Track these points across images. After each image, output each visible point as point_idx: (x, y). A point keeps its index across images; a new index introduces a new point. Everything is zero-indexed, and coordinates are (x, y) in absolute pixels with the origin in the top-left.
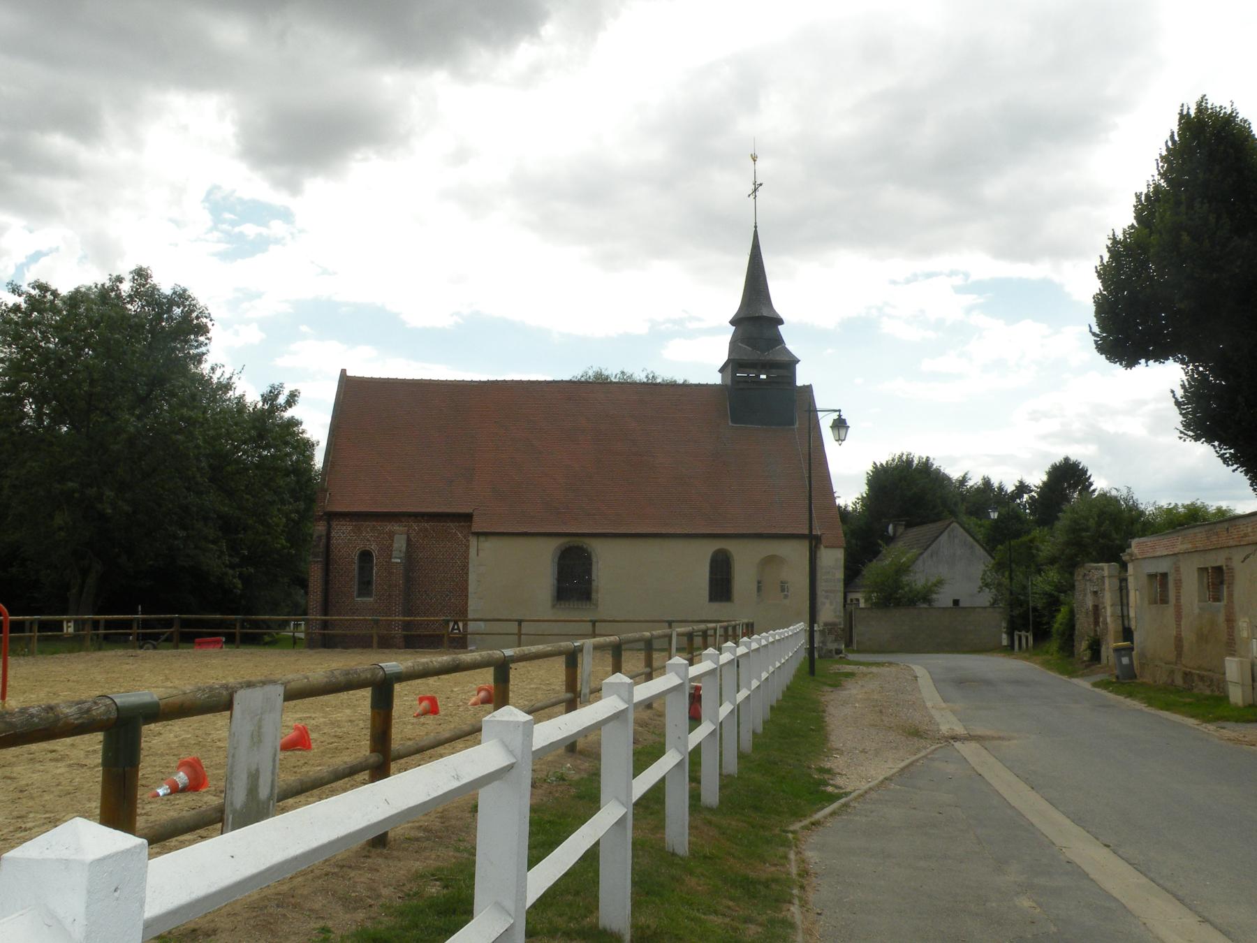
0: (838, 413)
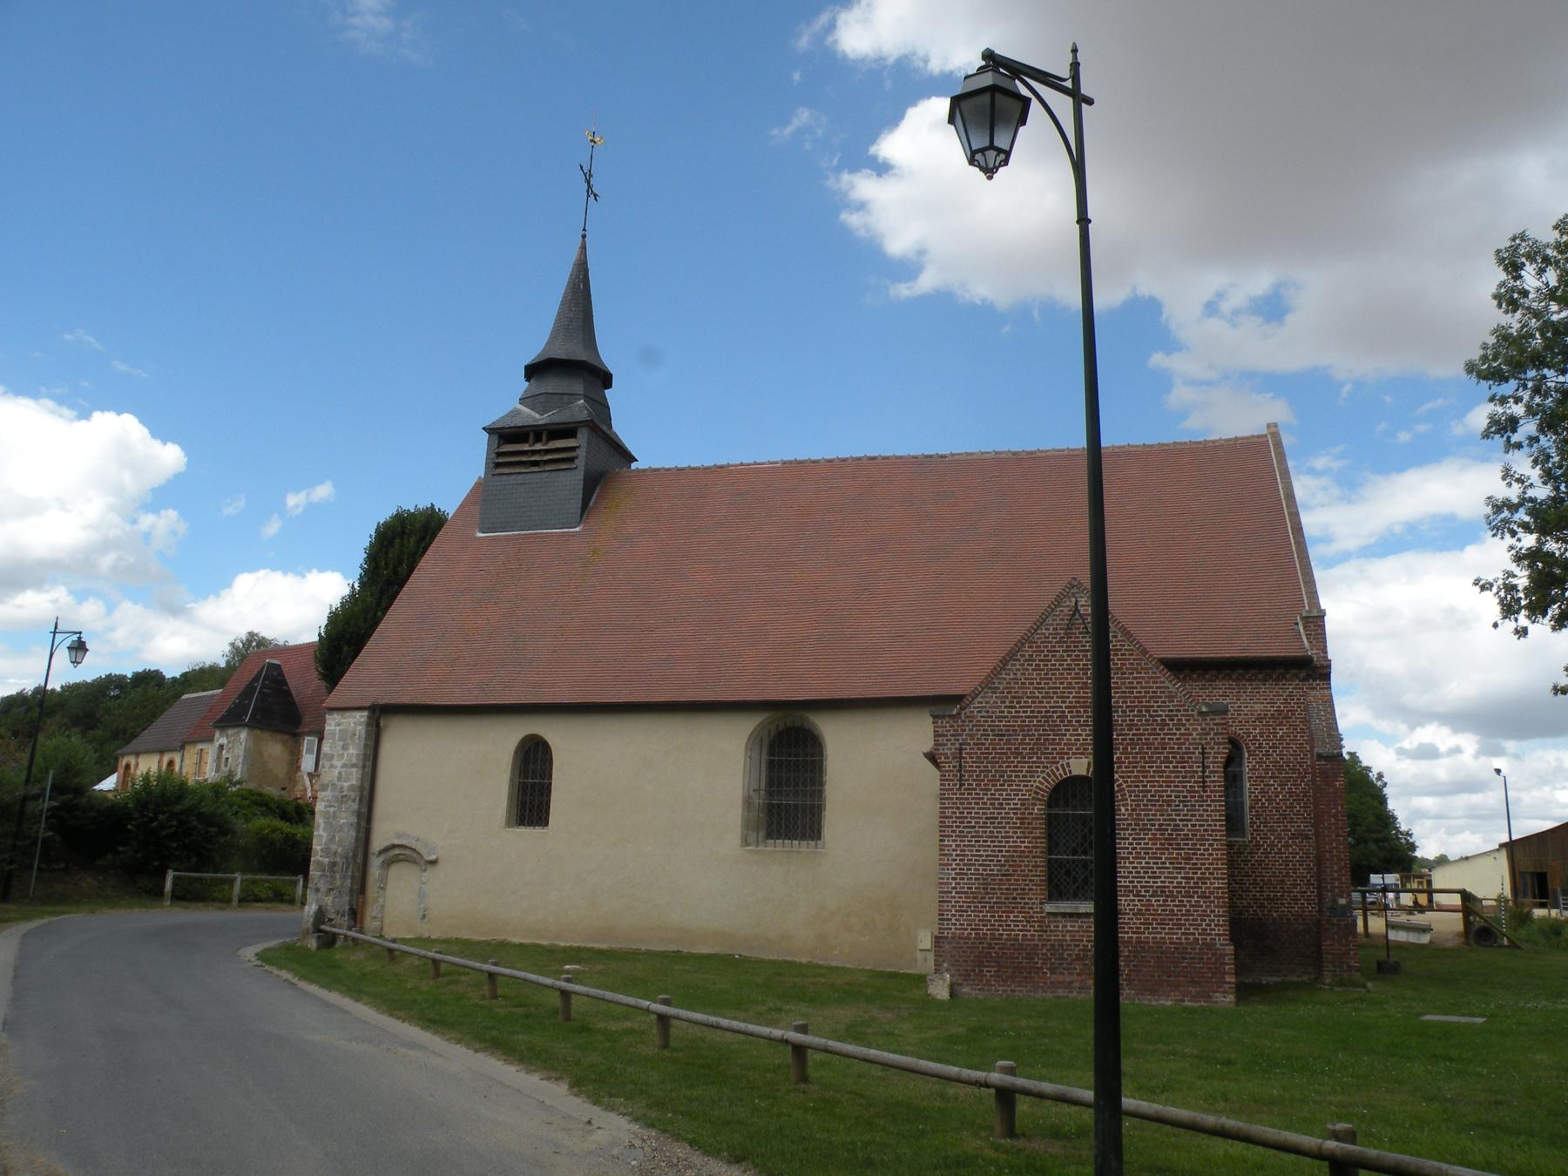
0: (78, 635)
